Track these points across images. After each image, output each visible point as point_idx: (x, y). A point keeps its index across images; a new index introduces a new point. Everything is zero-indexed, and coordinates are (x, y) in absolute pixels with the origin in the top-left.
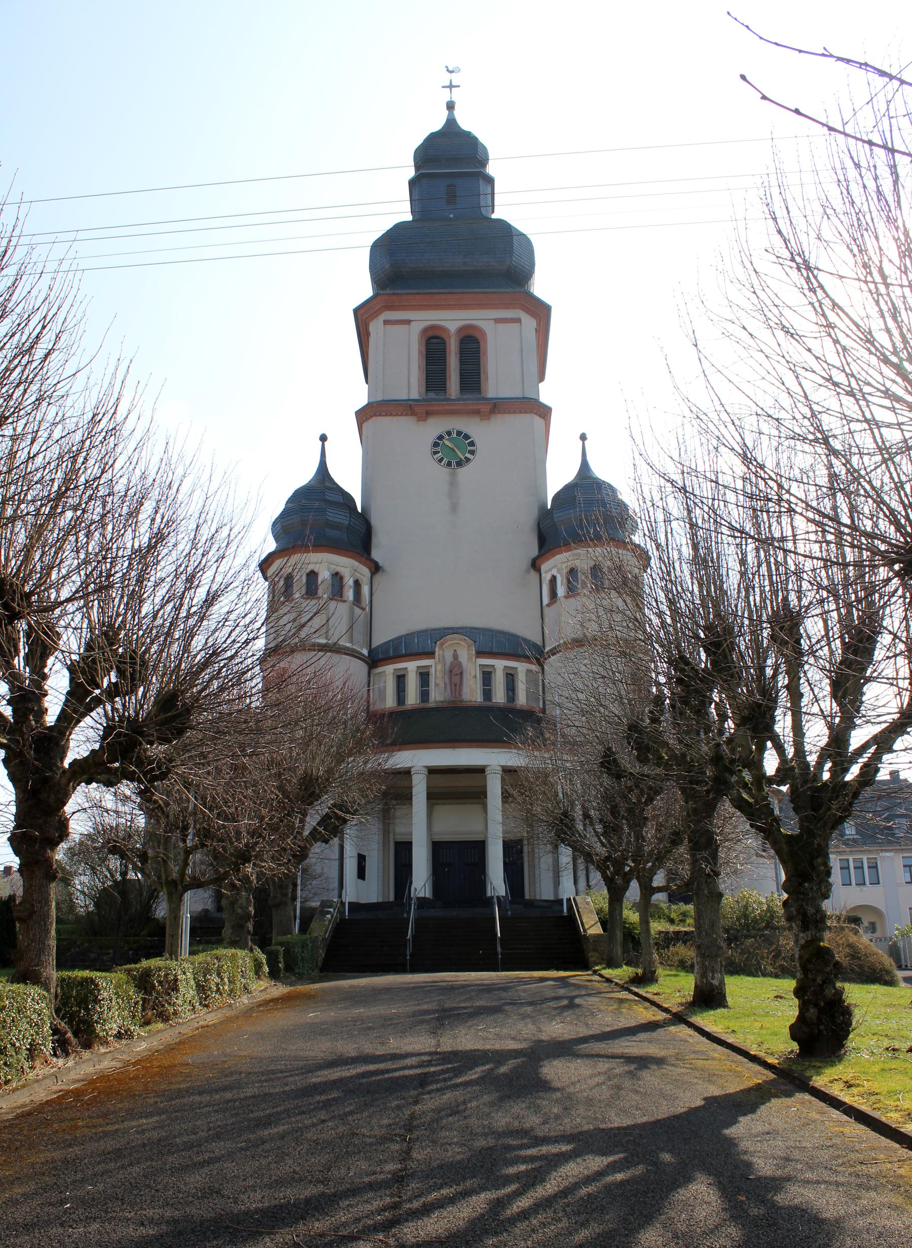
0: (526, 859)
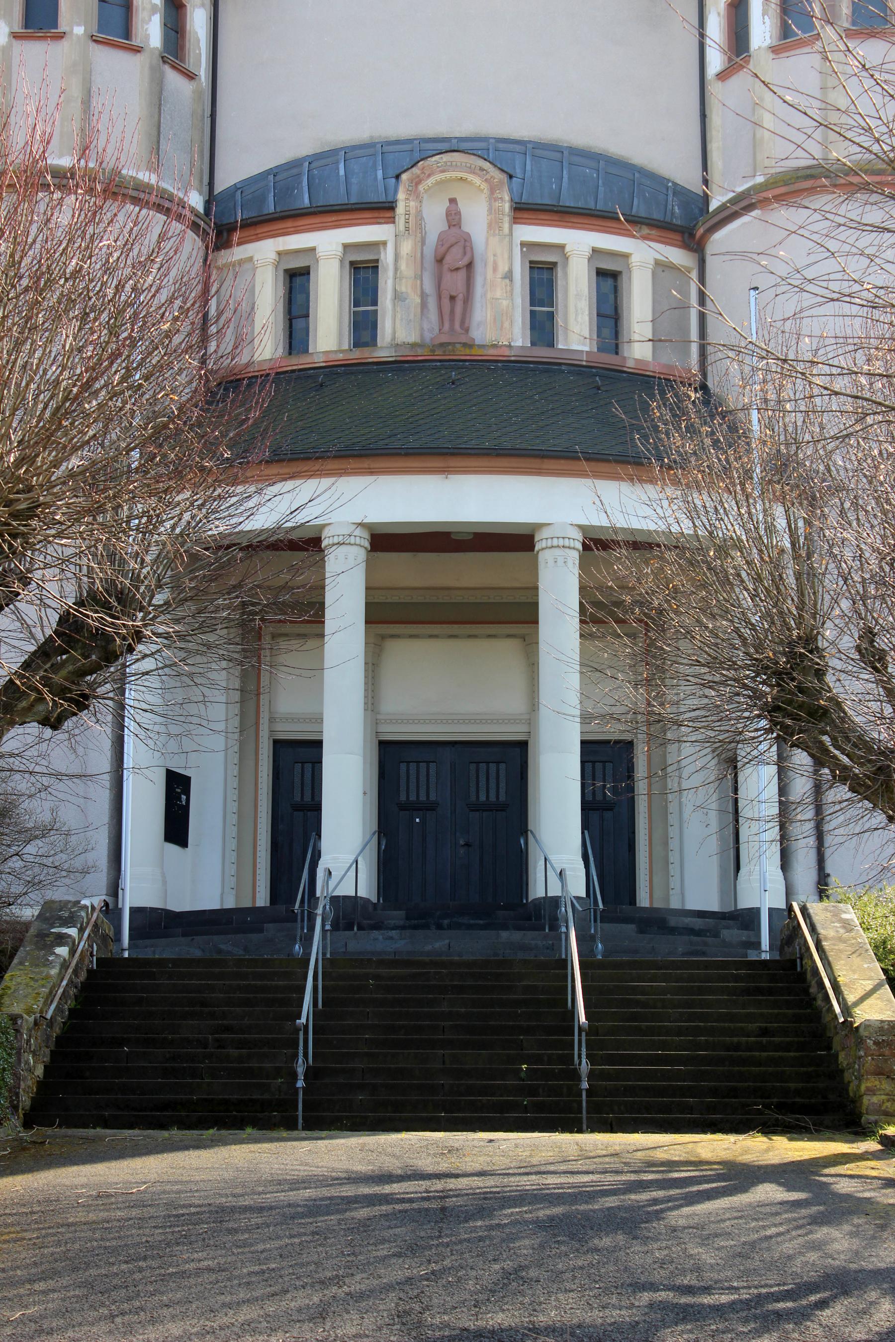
0: (641, 787)
